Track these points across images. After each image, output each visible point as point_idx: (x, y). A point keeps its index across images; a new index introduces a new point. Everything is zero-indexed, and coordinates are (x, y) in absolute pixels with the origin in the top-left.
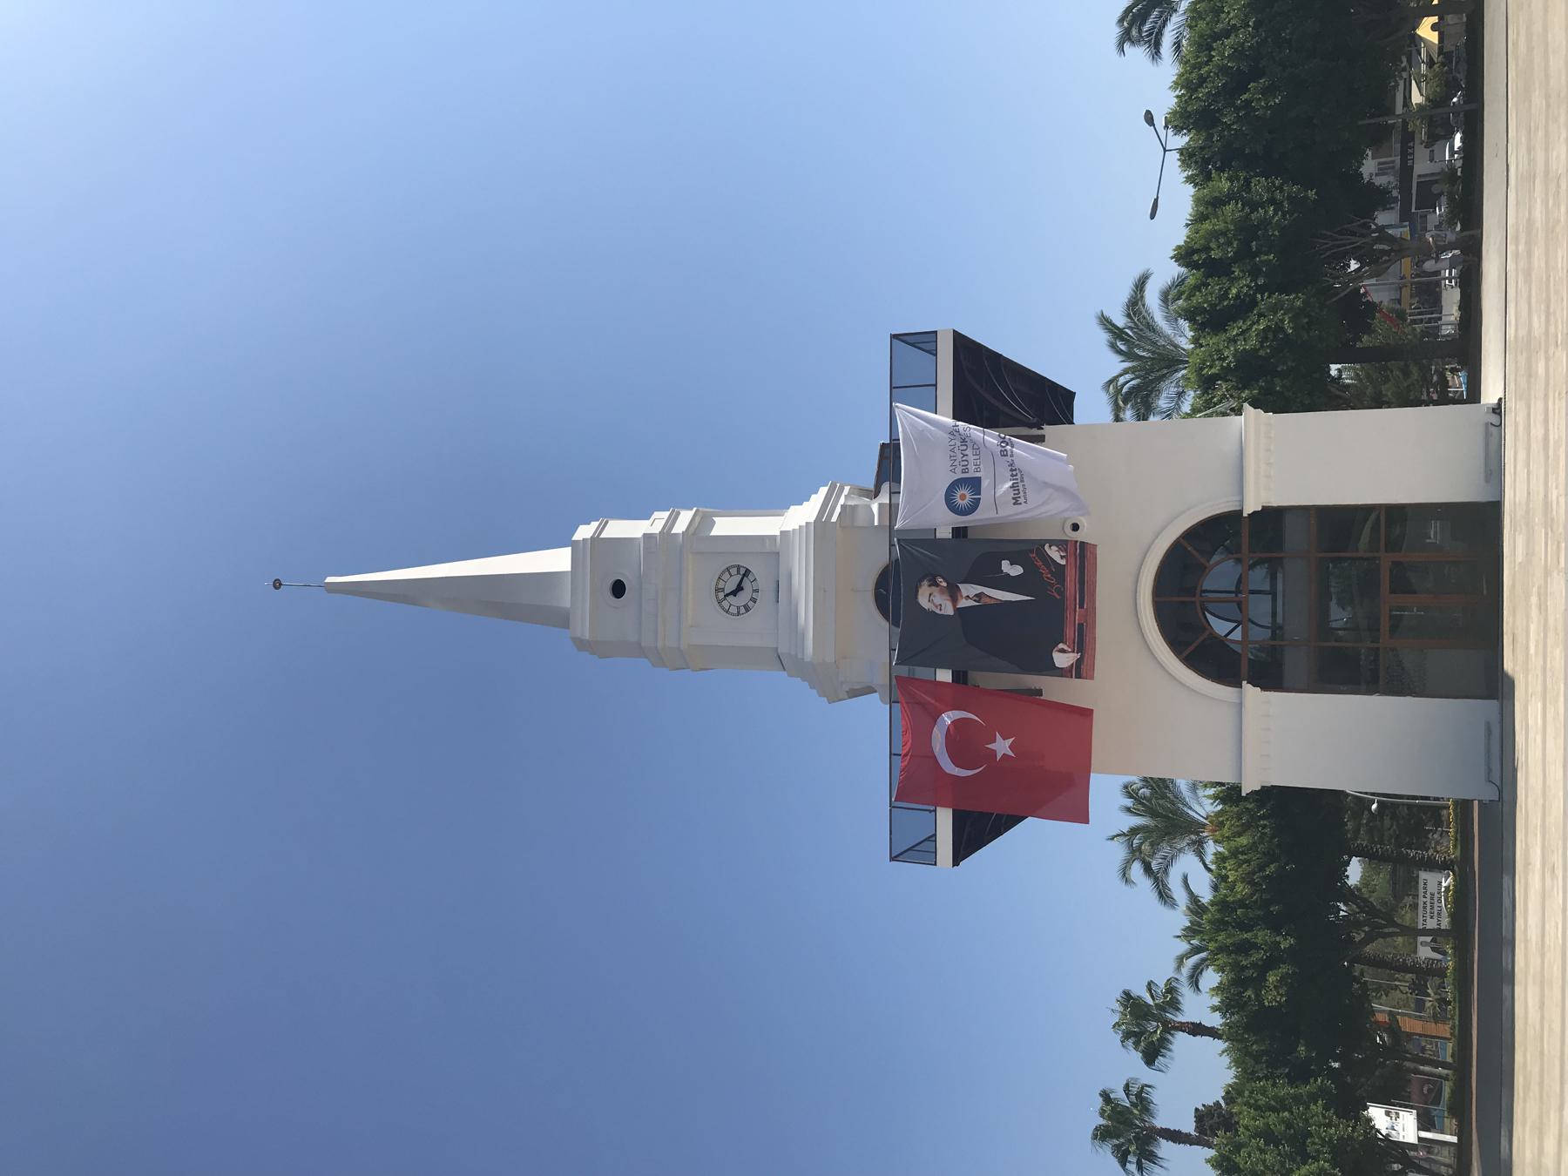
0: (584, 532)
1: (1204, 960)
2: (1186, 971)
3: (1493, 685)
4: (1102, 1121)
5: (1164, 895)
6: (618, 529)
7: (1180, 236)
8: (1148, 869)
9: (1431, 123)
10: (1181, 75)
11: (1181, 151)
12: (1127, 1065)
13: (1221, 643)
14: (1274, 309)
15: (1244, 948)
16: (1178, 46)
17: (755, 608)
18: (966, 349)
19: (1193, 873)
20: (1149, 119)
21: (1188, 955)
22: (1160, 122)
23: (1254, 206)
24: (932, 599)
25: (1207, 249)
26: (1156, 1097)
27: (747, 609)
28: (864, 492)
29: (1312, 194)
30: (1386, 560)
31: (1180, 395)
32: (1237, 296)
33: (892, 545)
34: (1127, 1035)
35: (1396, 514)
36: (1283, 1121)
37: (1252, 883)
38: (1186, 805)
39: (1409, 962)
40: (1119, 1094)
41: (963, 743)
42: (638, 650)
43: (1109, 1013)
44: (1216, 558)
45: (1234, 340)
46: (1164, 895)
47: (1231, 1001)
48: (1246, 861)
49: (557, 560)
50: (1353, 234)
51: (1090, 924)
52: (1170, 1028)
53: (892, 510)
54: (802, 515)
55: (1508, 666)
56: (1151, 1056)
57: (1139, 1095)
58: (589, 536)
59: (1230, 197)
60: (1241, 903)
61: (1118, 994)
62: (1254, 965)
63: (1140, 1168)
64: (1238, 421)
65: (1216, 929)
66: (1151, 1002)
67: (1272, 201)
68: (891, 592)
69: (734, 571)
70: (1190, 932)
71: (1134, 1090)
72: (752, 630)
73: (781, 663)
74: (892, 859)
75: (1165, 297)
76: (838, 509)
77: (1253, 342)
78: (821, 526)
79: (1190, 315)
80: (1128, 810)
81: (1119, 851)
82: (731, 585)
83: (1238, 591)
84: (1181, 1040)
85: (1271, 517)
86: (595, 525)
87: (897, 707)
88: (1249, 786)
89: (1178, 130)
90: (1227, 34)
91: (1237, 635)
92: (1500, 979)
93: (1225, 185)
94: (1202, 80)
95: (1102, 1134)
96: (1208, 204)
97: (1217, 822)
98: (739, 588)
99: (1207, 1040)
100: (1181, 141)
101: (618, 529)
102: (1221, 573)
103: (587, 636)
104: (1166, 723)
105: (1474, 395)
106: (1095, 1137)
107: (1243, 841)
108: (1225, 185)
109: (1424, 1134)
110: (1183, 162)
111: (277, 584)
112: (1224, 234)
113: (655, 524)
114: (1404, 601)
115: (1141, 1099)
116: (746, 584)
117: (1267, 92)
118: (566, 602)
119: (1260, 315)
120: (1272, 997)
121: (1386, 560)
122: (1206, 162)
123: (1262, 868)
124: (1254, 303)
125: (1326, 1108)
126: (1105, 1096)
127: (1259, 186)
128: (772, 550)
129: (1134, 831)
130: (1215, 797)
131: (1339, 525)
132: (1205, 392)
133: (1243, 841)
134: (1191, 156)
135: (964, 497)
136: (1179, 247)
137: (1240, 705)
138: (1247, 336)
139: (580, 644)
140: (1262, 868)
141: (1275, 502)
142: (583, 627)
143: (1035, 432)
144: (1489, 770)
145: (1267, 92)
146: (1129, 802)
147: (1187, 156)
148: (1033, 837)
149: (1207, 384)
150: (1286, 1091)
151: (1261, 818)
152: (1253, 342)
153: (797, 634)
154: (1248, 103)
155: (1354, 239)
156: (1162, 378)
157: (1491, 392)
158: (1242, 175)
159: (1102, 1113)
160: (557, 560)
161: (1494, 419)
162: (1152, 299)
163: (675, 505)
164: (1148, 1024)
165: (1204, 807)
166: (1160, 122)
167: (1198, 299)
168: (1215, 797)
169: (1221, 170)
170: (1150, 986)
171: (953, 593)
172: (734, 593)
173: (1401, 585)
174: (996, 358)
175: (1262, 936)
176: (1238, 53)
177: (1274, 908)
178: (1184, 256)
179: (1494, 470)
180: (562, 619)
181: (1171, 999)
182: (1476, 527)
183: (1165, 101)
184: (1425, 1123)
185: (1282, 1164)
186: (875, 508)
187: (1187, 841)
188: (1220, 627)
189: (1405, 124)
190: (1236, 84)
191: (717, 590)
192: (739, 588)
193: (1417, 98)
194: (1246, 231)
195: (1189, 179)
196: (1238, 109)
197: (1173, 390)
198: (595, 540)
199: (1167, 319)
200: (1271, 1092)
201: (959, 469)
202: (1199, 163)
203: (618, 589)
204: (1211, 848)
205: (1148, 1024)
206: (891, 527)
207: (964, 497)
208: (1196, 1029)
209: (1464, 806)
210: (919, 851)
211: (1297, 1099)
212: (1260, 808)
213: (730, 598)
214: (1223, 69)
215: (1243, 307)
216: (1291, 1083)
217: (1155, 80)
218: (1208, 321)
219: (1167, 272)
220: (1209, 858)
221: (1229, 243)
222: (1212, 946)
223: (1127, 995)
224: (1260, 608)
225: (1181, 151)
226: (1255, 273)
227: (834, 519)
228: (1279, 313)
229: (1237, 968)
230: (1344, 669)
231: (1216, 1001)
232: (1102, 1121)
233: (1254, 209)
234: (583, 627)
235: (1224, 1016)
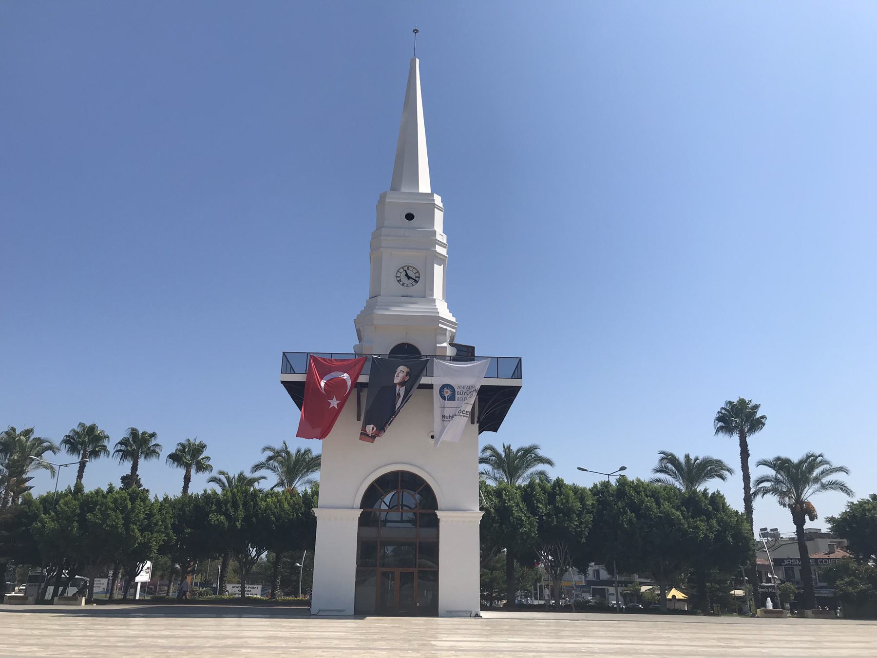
0: (438, 200)
1: (224, 484)
2: (218, 476)
3: (360, 613)
4: (140, 433)
5: (257, 467)
6: (439, 216)
7: (568, 481)
8: (270, 458)
9: (631, 595)
10: (642, 483)
11: (608, 482)
12: (168, 445)
13: (381, 497)
14: (531, 524)
15: (235, 505)
16: (658, 481)
17: (399, 285)
18: (512, 392)
19: (269, 481)
20: (623, 468)
21: (228, 479)
22: (622, 473)
23: (579, 516)
24: (401, 374)
25: (561, 494)
26: (153, 460)
27: (399, 281)
28: (452, 338)
29: (584, 540)
30: (415, 570)
31: (496, 479)
32: (538, 507)
33: (427, 356)
34: (183, 446)
35: (436, 574)
36: (157, 521)
37: (265, 510)
38: (301, 477)
39: (225, 579)
40: (153, 442)
41: (336, 387)
42: (380, 227)
43: (197, 438)
44: (417, 496)
45: (518, 505)
46: (257, 467)
47: (207, 498)
48: (276, 507)
49: (424, 185)
50: (566, 558)
51: (245, 434)
52: (188, 467)
53: (443, 357)
54: (443, 310)
55: (368, 618)
56: (175, 458)
57: (154, 451)
58: (436, 202)
59: (584, 505)
60: (256, 504)
61: (204, 442)
62: (227, 509)
63: (118, 451)
64: (477, 508)
65: (240, 489)
66: (201, 457)
67: (581, 523)
68: (406, 352)
69: (417, 275)
70: (241, 478)
71: (157, 449)
72: (389, 284)
73: (373, 297)
74: (284, 353)
75: (542, 473)
76: (445, 327)
77: (516, 514)
78: (437, 319)
79: (531, 485)
80: (299, 451)
81: (278, 446)
82: (410, 273)
83: (403, 505)
84: (182, 472)
85: (435, 523)
86: (441, 205)
87: (353, 357)
88: (317, 512)
89: (618, 481)
90: (658, 503)
91: (384, 507)
92: (239, 614)
93: (589, 503)
94: (638, 493)
95: (134, 433)
96: (582, 494)
97: (293, 493)
98: (409, 278)
99: (182, 484)
100: (613, 481)
101: (439, 216)
102: (411, 499)
103: (387, 200)
104: (343, 476)
105: (484, 608)
106: (133, 429)
107: (286, 506)
108: (589, 503)
109: (139, 585)
110: (604, 483)
111: (416, 31)
112: (567, 501)
113: (441, 237)
114: (398, 579)
115: (151, 453)
116: (411, 281)
117: (630, 522)
118: (404, 189)
119: (529, 517)
120: (213, 517)
121: (415, 570)
122: (603, 493)
123: (273, 514)
124: (534, 515)
125: (164, 540)
126: (153, 435)
127: (589, 518)
128: (426, 295)
129: (288, 453)
130: (306, 493)
131: (431, 550)
132: (495, 491)
133: (286, 506)
134: (606, 487)
135: (447, 392)
136: (562, 481)
137: (353, 508)
138: (519, 511)
139: (383, 197)
140: (273, 514)
141: (441, 524)
142: (391, 198)
143: (476, 420)
144: (324, 611)
145: (630, 522)
146: (302, 451)
147: (606, 485)
148: (294, 415)
149: (498, 493)
150: (169, 522)
151: (297, 514)
152: (516, 514)
153: (387, 306)
154: (626, 513)
155: (563, 559)
156: (504, 470)
157: (484, 614)
158: (595, 510)
159: (144, 433)
160: (424, 185)
161: (473, 614)
162: (540, 467)
163: (449, 246)
164: (189, 456)
165: (301, 487)
166: (622, 473)
167: (538, 489)
168: (306, 493)
169: (598, 500)
170: (208, 458)
171: (402, 384)
172: (407, 275)
173: (407, 578)
174: (511, 402)
175: (241, 514)
176: (648, 509)
177: (254, 519)
178: (559, 483)
179: (451, 614)
180: (395, 188)
181: (201, 468)
182: (429, 608)
183: (631, 476)
184: (143, 584)
185: (139, 521)
186: (445, 345)
187: (284, 478)
188: (387, 499)
189: (632, 583)
190: (635, 508)
191: (408, 267)
192: (409, 278)
193: (644, 588)
194: (568, 512)
195: (595, 486)
196: (624, 508)
197: (498, 475)
198: (434, 206)
199: (532, 473)
200: (168, 516)
201: (459, 390)
202: (601, 491)
203: (410, 217)
204: (279, 489)
205: (189, 456)
206: (435, 356)
207: (447, 392)
208: (187, 479)
209: (308, 603)
210: (287, 364)
211: (166, 527)
212: (302, 513)
213: (404, 273)
214: (642, 502)
215: (533, 510)
216: (173, 525)
217: (643, 470)
218: (528, 494)
219: (553, 474)
220: (276, 489)
221: (562, 504)
222: (235, 490)
223: (204, 446)
224: (394, 516)
225: (608, 482)
226: (548, 515)
227: (440, 325)
228: (529, 526)
229: (226, 502)
230: (367, 551)
231: (209, 492)
232: (140, 433)
233: (578, 515)
234: (391, 198)
235: (202, 495)
